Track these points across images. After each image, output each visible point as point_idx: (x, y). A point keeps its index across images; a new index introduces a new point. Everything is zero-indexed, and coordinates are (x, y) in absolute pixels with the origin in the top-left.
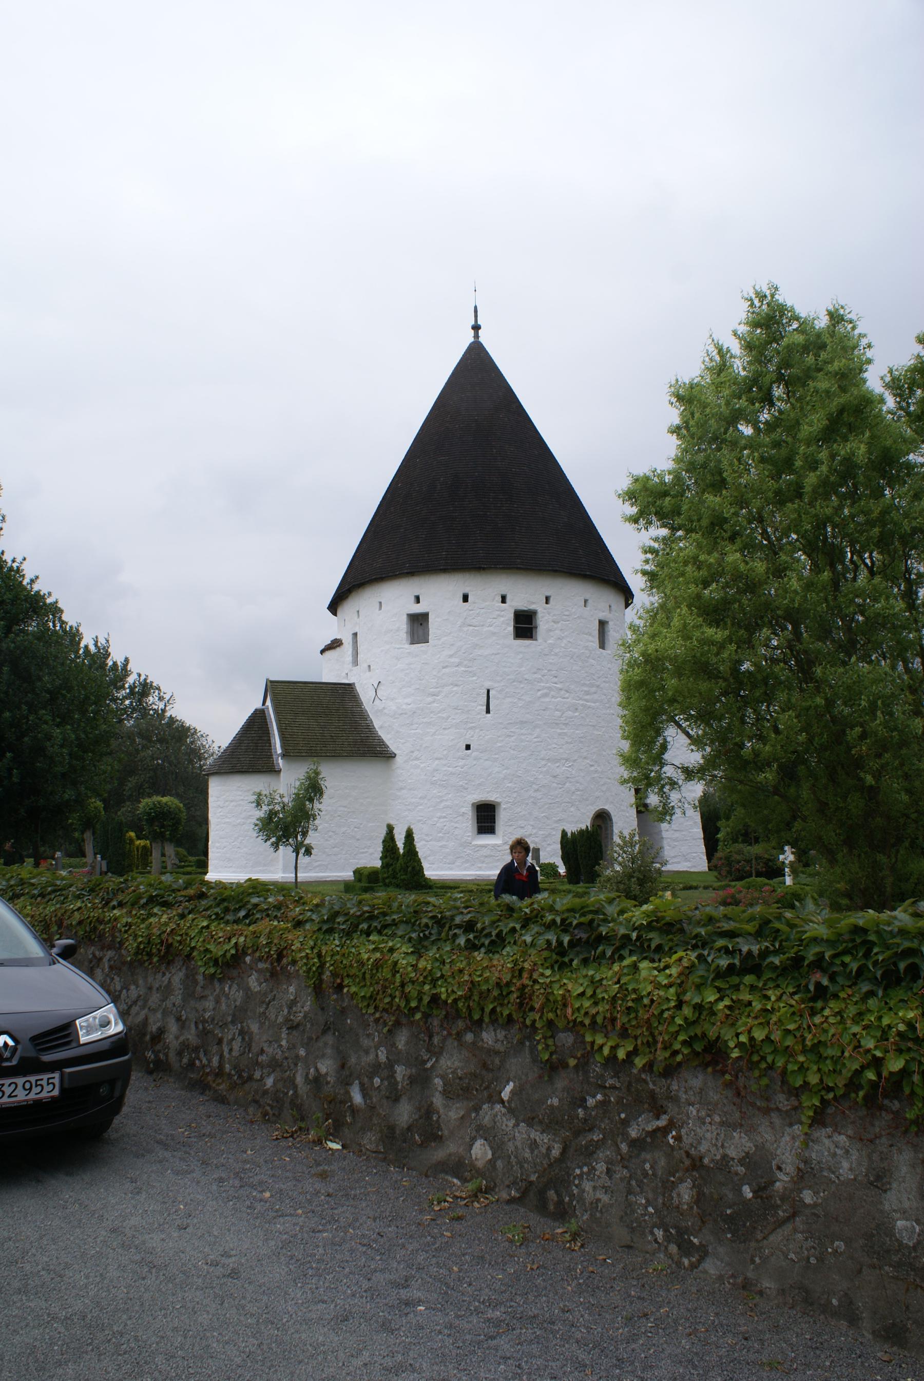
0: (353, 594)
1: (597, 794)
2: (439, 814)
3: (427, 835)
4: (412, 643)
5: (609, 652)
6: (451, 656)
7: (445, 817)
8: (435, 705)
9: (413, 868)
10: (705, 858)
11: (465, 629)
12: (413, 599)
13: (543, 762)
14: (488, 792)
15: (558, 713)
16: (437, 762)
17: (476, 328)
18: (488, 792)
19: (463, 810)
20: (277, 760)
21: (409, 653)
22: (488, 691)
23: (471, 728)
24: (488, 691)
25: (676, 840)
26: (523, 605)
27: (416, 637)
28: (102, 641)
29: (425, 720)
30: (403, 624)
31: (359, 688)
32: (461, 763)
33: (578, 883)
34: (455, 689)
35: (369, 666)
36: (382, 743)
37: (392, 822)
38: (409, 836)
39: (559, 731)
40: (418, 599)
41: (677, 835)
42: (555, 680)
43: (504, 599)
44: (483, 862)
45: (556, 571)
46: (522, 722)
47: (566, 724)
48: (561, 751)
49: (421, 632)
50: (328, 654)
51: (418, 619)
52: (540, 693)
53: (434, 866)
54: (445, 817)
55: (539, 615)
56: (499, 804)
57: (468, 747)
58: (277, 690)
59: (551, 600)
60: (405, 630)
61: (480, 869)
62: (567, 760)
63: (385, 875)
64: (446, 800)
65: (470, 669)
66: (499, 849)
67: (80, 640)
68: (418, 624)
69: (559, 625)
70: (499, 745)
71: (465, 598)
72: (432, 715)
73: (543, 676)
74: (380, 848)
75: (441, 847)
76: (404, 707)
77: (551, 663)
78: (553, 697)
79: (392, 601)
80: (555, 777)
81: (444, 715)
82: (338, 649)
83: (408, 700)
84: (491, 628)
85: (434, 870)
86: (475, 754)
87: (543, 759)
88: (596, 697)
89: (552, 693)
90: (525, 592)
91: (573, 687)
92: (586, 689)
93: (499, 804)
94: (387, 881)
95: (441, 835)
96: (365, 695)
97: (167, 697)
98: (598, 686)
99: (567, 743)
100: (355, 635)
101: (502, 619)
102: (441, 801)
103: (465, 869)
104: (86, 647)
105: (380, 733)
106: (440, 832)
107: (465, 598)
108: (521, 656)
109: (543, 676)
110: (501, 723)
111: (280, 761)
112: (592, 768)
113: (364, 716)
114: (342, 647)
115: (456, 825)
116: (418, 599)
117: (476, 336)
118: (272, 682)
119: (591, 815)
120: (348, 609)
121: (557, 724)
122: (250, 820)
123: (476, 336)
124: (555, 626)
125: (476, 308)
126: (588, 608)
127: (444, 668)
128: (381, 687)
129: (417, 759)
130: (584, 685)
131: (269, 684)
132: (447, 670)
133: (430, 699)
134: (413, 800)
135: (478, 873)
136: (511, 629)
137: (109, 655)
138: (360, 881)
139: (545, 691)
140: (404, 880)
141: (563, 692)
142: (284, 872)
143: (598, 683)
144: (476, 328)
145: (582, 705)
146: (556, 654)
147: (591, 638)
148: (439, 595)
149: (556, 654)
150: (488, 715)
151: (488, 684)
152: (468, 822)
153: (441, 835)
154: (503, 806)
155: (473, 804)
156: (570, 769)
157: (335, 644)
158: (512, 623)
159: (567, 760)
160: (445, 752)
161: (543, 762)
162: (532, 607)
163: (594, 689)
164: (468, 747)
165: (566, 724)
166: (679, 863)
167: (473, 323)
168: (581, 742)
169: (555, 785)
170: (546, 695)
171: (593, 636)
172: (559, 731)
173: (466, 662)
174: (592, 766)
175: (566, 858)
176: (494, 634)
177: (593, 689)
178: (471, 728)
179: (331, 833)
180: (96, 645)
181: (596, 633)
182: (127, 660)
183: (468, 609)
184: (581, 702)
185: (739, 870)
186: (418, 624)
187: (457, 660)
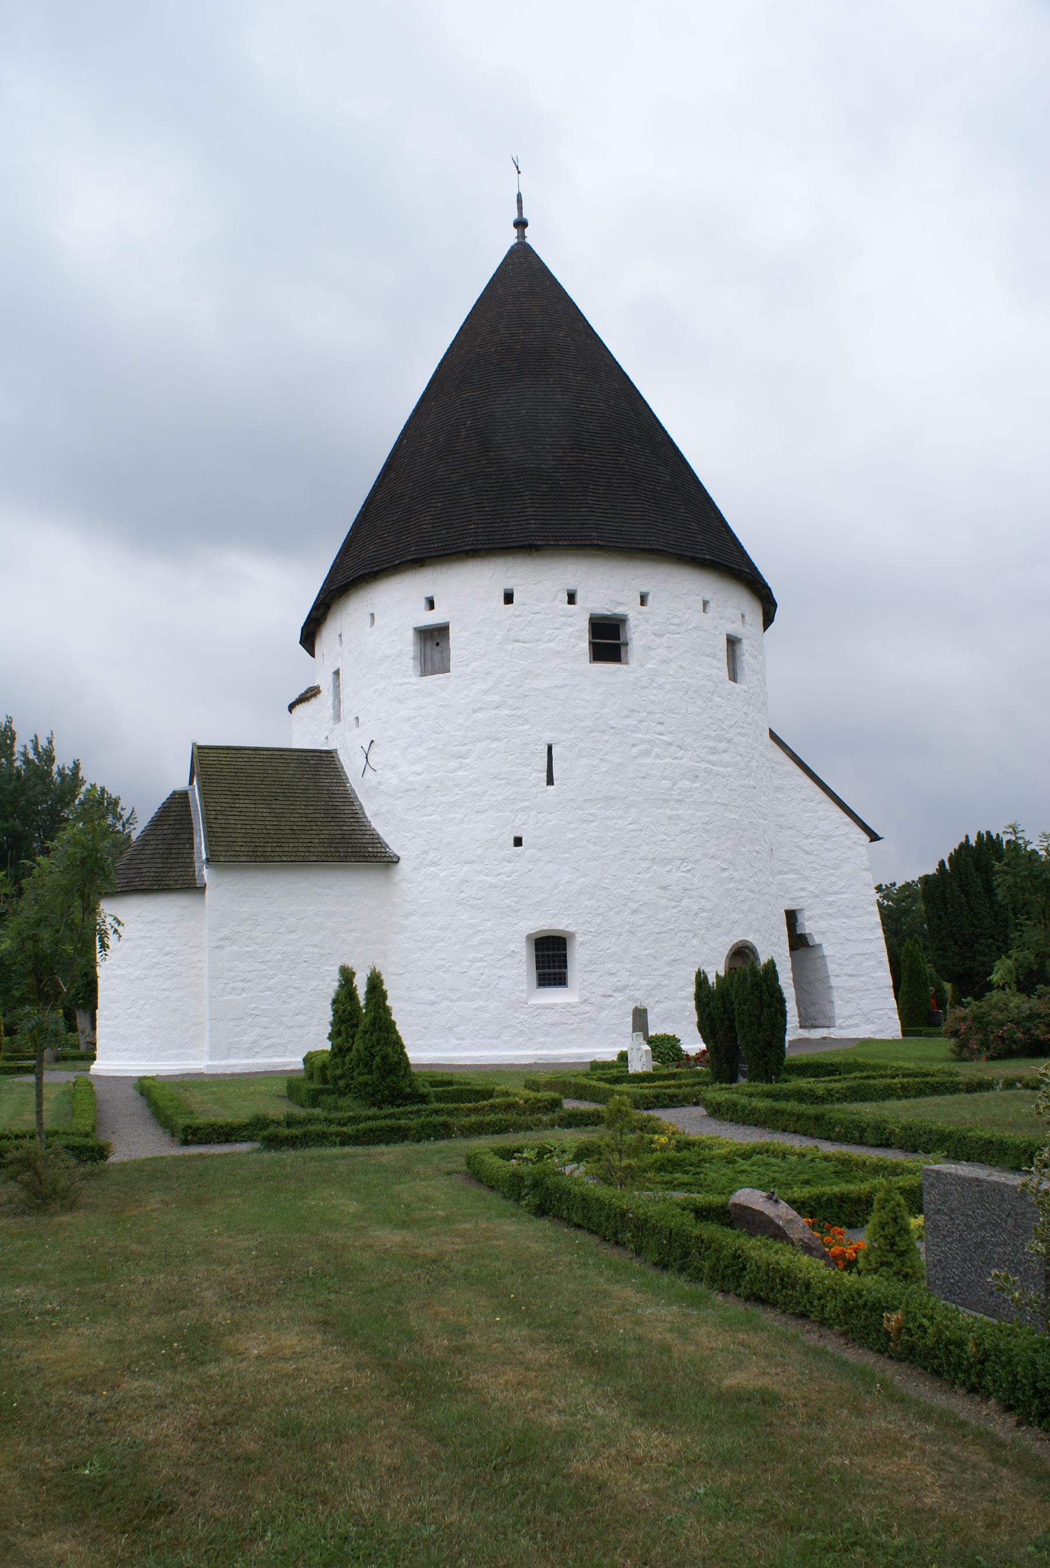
0: (332, 609)
1: (734, 916)
2: (471, 955)
3: (452, 990)
4: (424, 673)
5: (745, 687)
6: (486, 692)
7: (481, 960)
8: (462, 773)
9: (385, 1058)
10: (897, 1016)
11: (509, 647)
12: (423, 603)
13: (645, 864)
14: (554, 916)
15: (666, 783)
16: (467, 867)
17: (521, 224)
18: (554, 916)
19: (512, 947)
20: (201, 870)
21: (417, 690)
22: (550, 748)
23: (522, 810)
24: (550, 748)
25: (851, 990)
26: (604, 607)
27: (429, 665)
28: (43, 743)
29: (445, 799)
30: (408, 644)
31: (343, 757)
32: (508, 867)
33: (733, 1079)
34: (495, 745)
35: (357, 718)
36: (376, 840)
37: (350, 963)
38: (375, 985)
39: (668, 812)
40: (431, 604)
41: (853, 982)
42: (661, 728)
43: (571, 599)
44: (547, 1034)
45: (592, 546)
46: (608, 799)
47: (680, 801)
48: (674, 845)
49: (437, 657)
50: (299, 709)
51: (432, 637)
52: (635, 750)
53: (465, 1042)
54: (481, 960)
55: (632, 623)
56: (572, 935)
57: (518, 842)
58: (208, 761)
59: (650, 599)
60: (412, 654)
61: (543, 1046)
62: (683, 860)
63: (338, 1072)
64: (484, 931)
65: (519, 712)
66: (575, 1011)
67: (13, 739)
68: (433, 639)
69: (664, 640)
70: (570, 836)
71: (509, 598)
72: (456, 790)
73: (641, 721)
74: (328, 1015)
75: (476, 1009)
76: (411, 778)
77: (653, 702)
78: (658, 756)
79: (393, 608)
80: (664, 888)
81: (477, 790)
82: (313, 700)
83: (418, 768)
84: (552, 645)
85: (464, 1049)
86: (530, 852)
87: (644, 859)
88: (726, 757)
89: (656, 750)
90: (608, 585)
91: (688, 740)
92: (710, 744)
93: (572, 935)
94: (341, 1083)
95: (475, 989)
96: (351, 765)
97: (126, 815)
98: (729, 741)
99: (683, 832)
100: (337, 673)
101: (571, 629)
102: (475, 933)
103: (518, 1047)
104: (24, 754)
105: (374, 825)
106: (474, 985)
107: (509, 598)
108: (603, 689)
109: (641, 721)
110: (573, 800)
111: (205, 872)
112: (726, 874)
113: (348, 798)
114: (319, 697)
115: (501, 973)
116: (431, 604)
117: (522, 236)
118: (200, 748)
119: (726, 951)
120: (326, 640)
121: (665, 801)
122: (619, 997)
123: (522, 236)
124: (658, 641)
125: (519, 196)
126: (710, 615)
127: (475, 711)
128: (374, 749)
129: (433, 864)
130: (707, 737)
131: (196, 751)
132: (480, 715)
133: (453, 764)
134: (429, 932)
135: (539, 1052)
136: (584, 645)
137: (53, 760)
138: (311, 1076)
139: (645, 746)
140: (366, 1084)
141: (673, 749)
142: (211, 1058)
143: (729, 736)
144: (521, 224)
145: (705, 770)
146: (661, 687)
147: (715, 663)
148: (464, 592)
149: (661, 687)
150: (551, 788)
151: (549, 737)
152: (522, 965)
153: (475, 989)
154: (579, 939)
155: (529, 937)
156: (689, 875)
157: (310, 694)
158: (586, 636)
159: (683, 860)
160: (480, 851)
161: (645, 864)
162: (619, 610)
163: (723, 745)
164: (518, 842)
165: (680, 801)
166: (857, 1025)
167: (515, 216)
168: (707, 831)
169: (664, 902)
170: (646, 753)
171: (719, 660)
172: (668, 812)
173: (511, 701)
174: (724, 870)
175: (707, 1027)
176: (557, 653)
177: (723, 745)
178: (522, 810)
179: (291, 991)
180: (35, 748)
181: (723, 655)
182: (77, 766)
183: (511, 615)
184: (704, 765)
185: (1002, 1038)
186: (433, 639)
187: (496, 698)
